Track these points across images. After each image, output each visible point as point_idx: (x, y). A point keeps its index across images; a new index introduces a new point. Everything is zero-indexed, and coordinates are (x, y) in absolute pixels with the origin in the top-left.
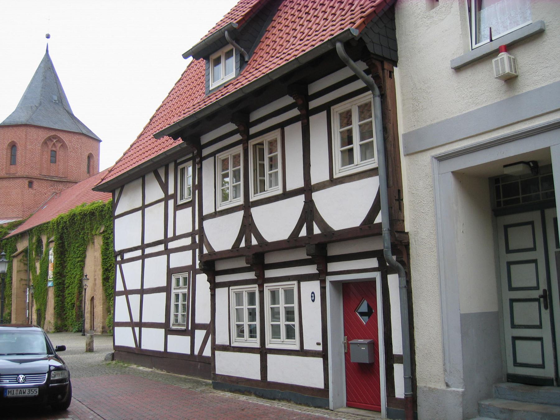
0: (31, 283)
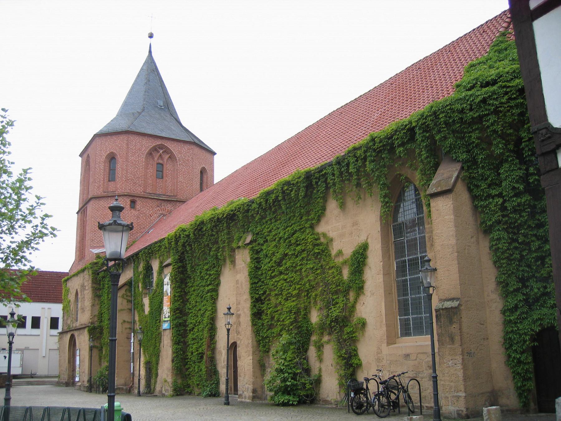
0: (137, 327)
